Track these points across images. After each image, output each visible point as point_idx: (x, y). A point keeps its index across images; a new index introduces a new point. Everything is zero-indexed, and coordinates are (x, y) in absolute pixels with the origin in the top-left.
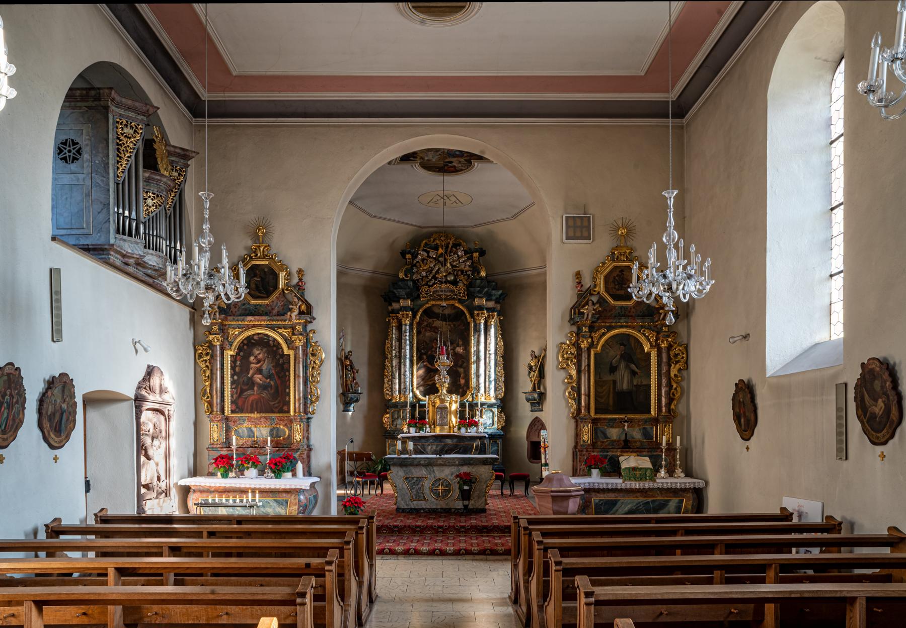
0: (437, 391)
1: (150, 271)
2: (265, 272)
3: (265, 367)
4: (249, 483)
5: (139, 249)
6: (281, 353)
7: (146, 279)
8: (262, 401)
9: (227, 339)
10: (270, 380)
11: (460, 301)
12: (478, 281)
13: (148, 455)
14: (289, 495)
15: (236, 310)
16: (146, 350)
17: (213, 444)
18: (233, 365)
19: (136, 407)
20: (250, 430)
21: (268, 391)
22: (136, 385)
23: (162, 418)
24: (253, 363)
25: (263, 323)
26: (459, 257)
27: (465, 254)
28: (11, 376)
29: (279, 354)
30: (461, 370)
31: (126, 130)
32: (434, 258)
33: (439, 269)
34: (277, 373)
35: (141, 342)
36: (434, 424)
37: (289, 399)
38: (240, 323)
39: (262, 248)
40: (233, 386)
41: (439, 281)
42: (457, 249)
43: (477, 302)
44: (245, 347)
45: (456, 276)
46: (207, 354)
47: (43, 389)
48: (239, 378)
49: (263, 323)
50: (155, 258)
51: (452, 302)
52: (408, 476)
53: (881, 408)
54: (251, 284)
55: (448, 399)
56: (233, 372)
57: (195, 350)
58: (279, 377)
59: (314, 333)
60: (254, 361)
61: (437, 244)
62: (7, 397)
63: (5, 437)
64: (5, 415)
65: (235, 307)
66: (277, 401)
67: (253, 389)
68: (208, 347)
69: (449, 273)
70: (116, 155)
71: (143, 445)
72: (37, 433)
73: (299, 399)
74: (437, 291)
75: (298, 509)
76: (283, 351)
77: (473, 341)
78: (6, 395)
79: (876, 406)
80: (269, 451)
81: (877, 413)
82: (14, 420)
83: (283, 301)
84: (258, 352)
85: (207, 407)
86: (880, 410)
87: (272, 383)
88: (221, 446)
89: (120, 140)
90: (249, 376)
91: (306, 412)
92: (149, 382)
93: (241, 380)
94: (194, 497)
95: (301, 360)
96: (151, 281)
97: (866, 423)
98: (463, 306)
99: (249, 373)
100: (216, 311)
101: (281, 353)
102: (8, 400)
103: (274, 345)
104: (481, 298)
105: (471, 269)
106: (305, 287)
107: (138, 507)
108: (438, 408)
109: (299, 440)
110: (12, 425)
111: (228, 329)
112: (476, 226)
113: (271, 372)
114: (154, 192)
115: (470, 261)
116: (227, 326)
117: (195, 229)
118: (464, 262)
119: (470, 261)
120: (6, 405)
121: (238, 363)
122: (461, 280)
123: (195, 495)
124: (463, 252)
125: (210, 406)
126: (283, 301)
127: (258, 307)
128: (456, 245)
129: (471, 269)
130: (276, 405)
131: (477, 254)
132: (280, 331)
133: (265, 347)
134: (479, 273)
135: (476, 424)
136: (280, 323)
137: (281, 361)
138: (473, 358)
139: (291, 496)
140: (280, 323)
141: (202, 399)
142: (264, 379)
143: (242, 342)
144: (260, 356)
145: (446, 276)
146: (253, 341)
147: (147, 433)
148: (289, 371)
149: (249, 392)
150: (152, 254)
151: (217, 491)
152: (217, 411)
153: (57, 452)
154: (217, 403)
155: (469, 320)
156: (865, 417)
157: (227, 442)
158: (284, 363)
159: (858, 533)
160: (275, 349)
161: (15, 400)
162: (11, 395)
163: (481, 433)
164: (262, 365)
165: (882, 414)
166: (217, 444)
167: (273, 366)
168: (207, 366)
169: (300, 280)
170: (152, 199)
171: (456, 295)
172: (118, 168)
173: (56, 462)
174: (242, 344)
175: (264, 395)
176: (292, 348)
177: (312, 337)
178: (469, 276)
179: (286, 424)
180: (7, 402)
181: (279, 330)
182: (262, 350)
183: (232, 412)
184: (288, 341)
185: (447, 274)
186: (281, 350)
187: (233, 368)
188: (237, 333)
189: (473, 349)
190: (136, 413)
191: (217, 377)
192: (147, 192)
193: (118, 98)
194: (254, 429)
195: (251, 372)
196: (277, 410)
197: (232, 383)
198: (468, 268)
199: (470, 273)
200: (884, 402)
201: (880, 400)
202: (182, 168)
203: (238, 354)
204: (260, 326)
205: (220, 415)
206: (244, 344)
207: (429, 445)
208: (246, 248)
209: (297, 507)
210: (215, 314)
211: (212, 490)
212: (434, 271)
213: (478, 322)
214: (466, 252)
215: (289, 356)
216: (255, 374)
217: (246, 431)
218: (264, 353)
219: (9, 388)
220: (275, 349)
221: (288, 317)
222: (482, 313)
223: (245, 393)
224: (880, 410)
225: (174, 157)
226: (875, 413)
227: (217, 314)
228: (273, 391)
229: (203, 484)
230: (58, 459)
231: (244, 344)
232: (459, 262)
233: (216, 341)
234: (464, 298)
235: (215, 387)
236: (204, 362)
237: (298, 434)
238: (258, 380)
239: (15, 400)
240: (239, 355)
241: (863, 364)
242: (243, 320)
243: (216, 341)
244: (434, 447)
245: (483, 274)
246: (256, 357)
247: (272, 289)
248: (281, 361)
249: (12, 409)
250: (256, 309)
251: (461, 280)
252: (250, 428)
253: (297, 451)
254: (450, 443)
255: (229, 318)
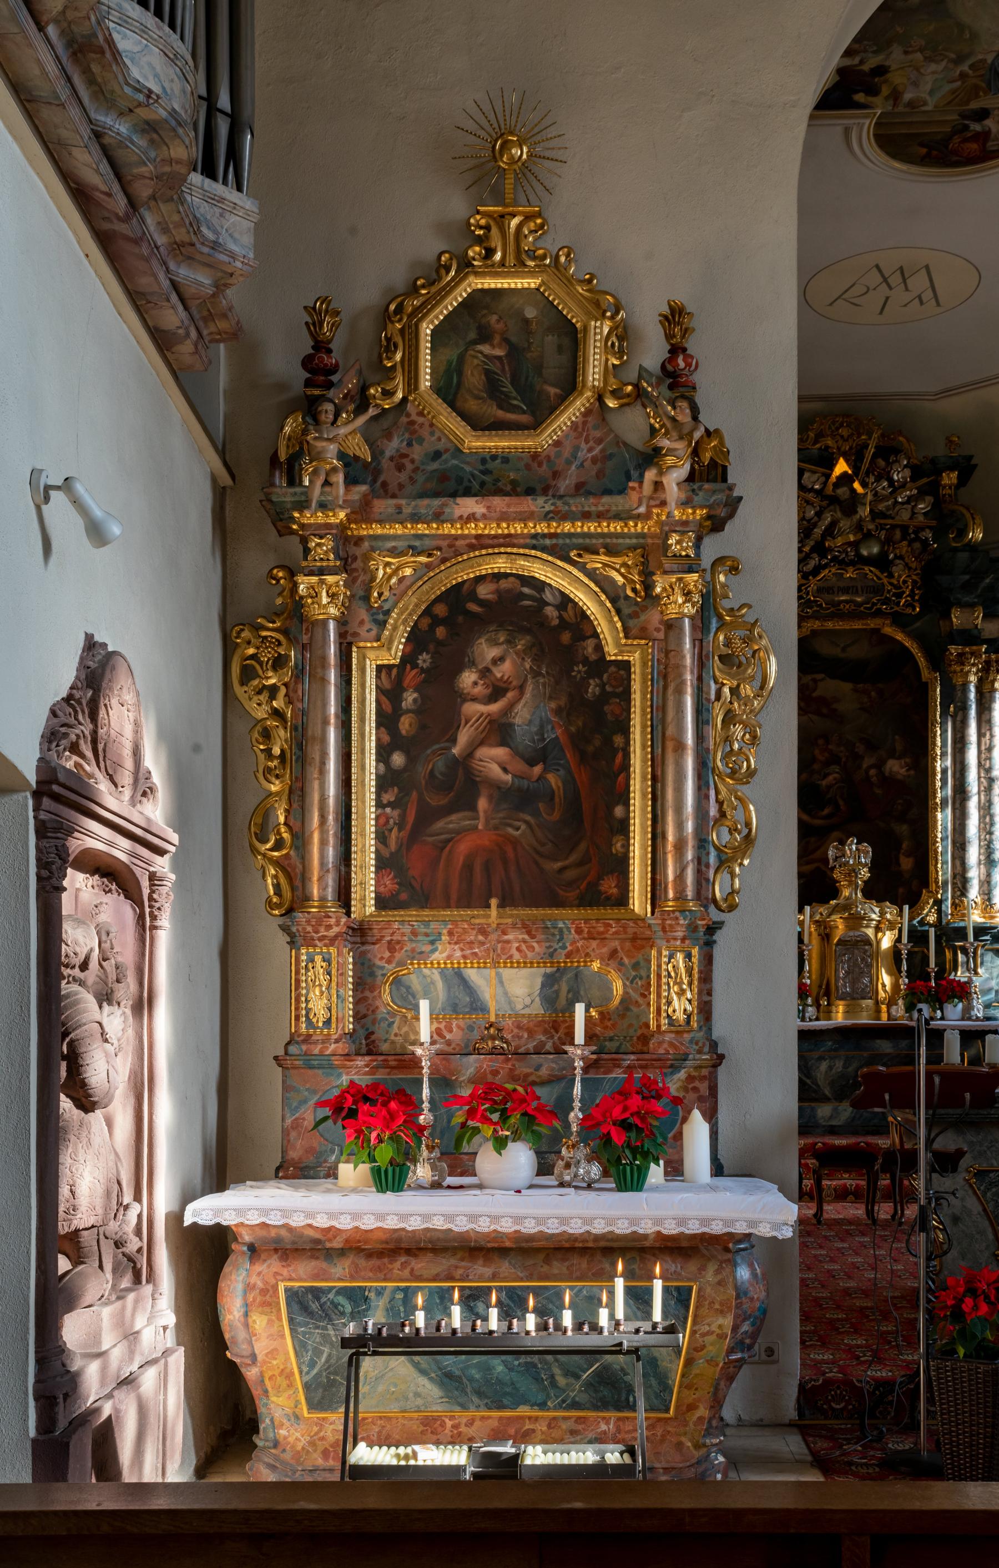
0: (835, 893)
1: (122, 128)
2: (527, 322)
3: (522, 715)
4: (423, 1209)
6: (593, 657)
8: (511, 854)
9: (366, 598)
10: (545, 770)
11: (899, 620)
12: (963, 556)
13: (83, 1084)
14: (692, 1266)
15: (403, 477)
16: (96, 533)
17: (307, 1039)
18: (387, 707)
19: (42, 831)
20: (457, 979)
21: (536, 814)
22: (38, 721)
23: (128, 911)
24: (474, 699)
25: (518, 528)
26: (896, 488)
27: (914, 478)
29: (585, 661)
30: (903, 829)
32: (816, 491)
33: (834, 524)
34: (578, 740)
35: (79, 488)
36: (828, 994)
37: (627, 846)
38: (421, 528)
39: (515, 222)
40: (388, 797)
41: (835, 559)
42: (889, 464)
43: (957, 618)
44: (441, 632)
45: (888, 542)
46: (278, 663)
48: (411, 760)
49: (518, 528)
50: (155, 58)
51: (872, 624)
52: (984, 1167)
54: (468, 371)
55: (874, 916)
56: (386, 738)
57: (229, 648)
58: (583, 757)
59: (734, 570)
60: (479, 690)
61: (827, 447)
65: (400, 468)
66: (573, 858)
67: (473, 808)
68: (284, 631)
69: (868, 536)
71: (65, 1034)
73: (680, 847)
74: (829, 590)
75: (735, 1328)
76: (599, 648)
77: (942, 738)
80: (579, 1064)
83: (599, 441)
84: (493, 652)
85: (277, 887)
87: (553, 780)
88: (342, 1048)
90: (455, 751)
91: (704, 896)
92: (94, 717)
93: (422, 771)
94: (254, 1279)
95: (688, 677)
98: (909, 635)
99: (454, 741)
100: (334, 470)
101: (593, 657)
103: (564, 625)
104: (972, 606)
105: (934, 523)
106: (697, 378)
107: (40, 1361)
108: (840, 942)
109: (680, 1016)
111: (367, 558)
112: (947, 393)
113: (549, 736)
115: (929, 499)
116: (366, 544)
118: (908, 502)
119: (929, 499)
121: (409, 698)
122: (901, 557)
123: (259, 1267)
124: (907, 472)
125: (290, 878)
126: (599, 441)
127: (491, 465)
128: (888, 452)
129: (934, 523)
130: (571, 874)
131: (954, 475)
132: (596, 562)
133: (528, 631)
134: (962, 532)
135: (963, 992)
136: (591, 527)
137: (593, 689)
138: (943, 791)
139: (703, 1268)
140: (591, 527)
141: (254, 851)
142: (520, 766)
143: (427, 612)
144: (505, 670)
145: (856, 545)
146: (473, 607)
147: (76, 972)
148: (624, 729)
149: (455, 821)
151: (359, 1250)
152: (323, 899)
154: (322, 863)
155: (926, 674)
157: (362, 1033)
158: (604, 697)
160: (566, 637)
163: (978, 1019)
164: (511, 706)
166: (326, 1040)
167: (558, 712)
168: (277, 713)
169: (676, 350)
171: (886, 601)
174: (426, 622)
175: (519, 831)
176: (643, 633)
177: (723, 586)
178: (925, 543)
179: (613, 954)
181: (587, 558)
182: (508, 642)
183: (382, 903)
184: (622, 603)
185: (859, 536)
186: (590, 643)
187: (386, 720)
188: (408, 572)
189: (942, 763)
190: (41, 864)
191: (324, 755)
194: (472, 974)
195: (464, 737)
196: (572, 895)
197: (383, 784)
198: (921, 518)
199: (929, 534)
203: (408, 659)
204: (508, 540)
205: (337, 923)
206: (437, 621)
207: (821, 1058)
208: (442, 228)
209: (727, 1322)
210: (327, 483)
211: (337, 1244)
212: (818, 531)
213: (959, 681)
214: (917, 472)
215: (626, 665)
216: (482, 743)
217: (440, 985)
218: (522, 655)
220: (566, 637)
221: (647, 488)
222: (972, 654)
223: (440, 824)
227: (339, 478)
228: (556, 816)
229: (297, 1221)
231: (437, 621)
232: (896, 502)
233: (325, 600)
234: (909, 611)
235: (316, 797)
236: (264, 697)
237: (681, 993)
238: (495, 771)
240: (414, 666)
242: (439, 517)
243: (325, 600)
244: (839, 1065)
245: (976, 535)
246: (485, 673)
247: (553, 391)
248: (593, 689)
250: (486, 472)
251: (901, 557)
252: (459, 975)
253: (675, 1069)
254: (889, 1050)
255: (383, 506)
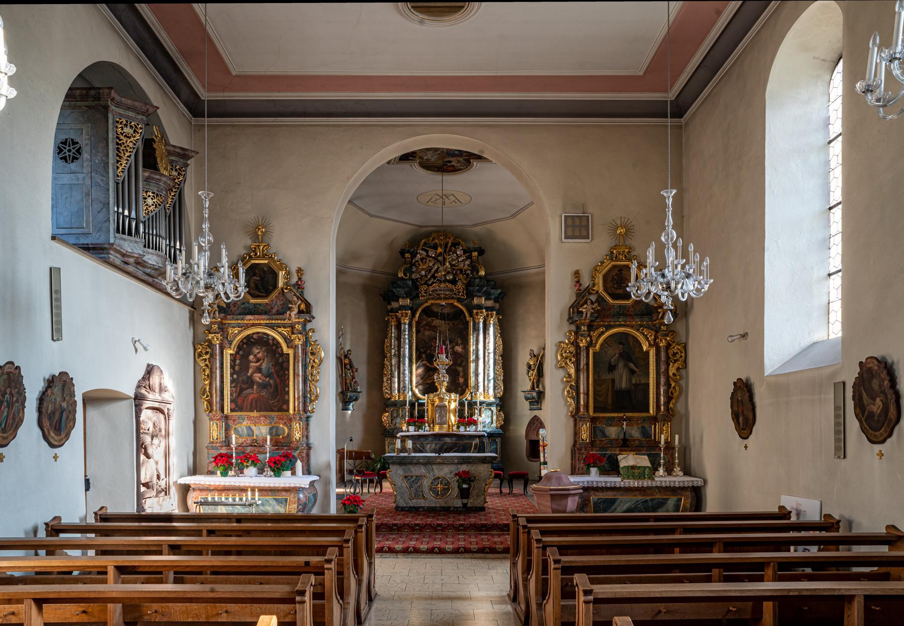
0: (436, 390)
1: (149, 270)
2: (264, 271)
3: (264, 366)
4: (248, 481)
5: (138, 248)
6: (281, 352)
7: (146, 278)
8: (262, 400)
9: (227, 338)
10: (270, 379)
11: (459, 300)
12: (477, 281)
13: (148, 454)
14: (289, 494)
15: (236, 309)
16: (145, 349)
17: (212, 443)
18: (233, 364)
19: (136, 406)
20: (249, 428)
21: (267, 389)
22: (135, 384)
23: (162, 416)
24: (253, 362)
25: (262, 322)
26: (458, 257)
27: (464, 254)
28: (11, 375)
29: (279, 353)
30: (460, 369)
31: (125, 130)
32: (433, 257)
33: (438, 268)
34: (277, 372)
35: (141, 341)
36: (433, 422)
37: (289, 397)
38: (240, 322)
39: (261, 248)
40: (233, 385)
41: (438, 280)
42: (456, 249)
43: (476, 301)
44: (245, 346)
45: (455, 275)
46: (207, 353)
47: (43, 388)
48: (238, 376)
49: (262, 322)
50: (155, 258)
51: (451, 301)
52: (407, 475)
53: (879, 406)
54: (251, 283)
55: (447, 398)
56: (232, 371)
57: (195, 349)
58: (278, 376)
59: (313, 331)
60: (254, 360)
61: (436, 243)
62: (7, 396)
63: (5, 435)
64: (5, 414)
65: (235, 306)
66: (276, 400)
67: (253, 388)
68: (208, 345)
69: (449, 273)
70: (115, 155)
71: (143, 444)
72: (37, 431)
73: (299, 398)
74: (436, 290)
75: (298, 507)
76: (282, 350)
77: (472, 340)
78: (6, 394)
79: (874, 405)
80: (268, 449)
81: (875, 411)
82: (14, 418)
83: (282, 300)
84: (257, 351)
85: (207, 406)
86: (878, 409)
87: (271, 381)
88: (220, 445)
89: (120, 140)
90: (249, 374)
91: (305, 411)
92: (149, 380)
93: (241, 379)
94: (194, 496)
95: (300, 359)
96: (150, 280)
97: (864, 422)
98: (462, 305)
99: (248, 372)
100: (216, 310)
101: (281, 352)
102: (8, 399)
103: (273, 344)
104: (480, 297)
105: (470, 268)
106: (305, 286)
107: (137, 505)
108: (437, 406)
109: (298, 438)
110: (12, 424)
111: (227, 328)
112: (475, 225)
113: (270, 371)
114: (154, 191)
115: (469, 260)
116: (227, 325)
117: (195, 228)
118: (463, 261)
119: (469, 260)
120: (6, 404)
121: (238, 362)
122: (460, 279)
123: (194, 493)
124: (462, 252)
125: (210, 404)
126: (282, 300)
127: (257, 306)
128: (455, 245)
129: (470, 268)
130: (276, 404)
131: (476, 253)
132: (280, 330)
133: (265, 346)
134: (478, 272)
135: (475, 423)
136: (279, 322)
137: (281, 360)
138: (472, 357)
139: (291, 494)
140: (279, 322)
141: (201, 398)
142: (263, 378)
143: (242, 341)
144: (260, 355)
145: (445, 275)
146: (252, 340)
147: (147, 431)
148: (288, 370)
149: (249, 391)
150: (152, 254)
151: (217, 490)
152: (216, 410)
153: (56, 450)
154: (216, 402)
155: (468, 319)
156: (863, 416)
157: (227, 441)
158: (283, 362)
159: (856, 531)
160: (274, 347)
161: (15, 399)
162: (11, 394)
163: (480, 431)
164: (261, 364)
165: (880, 413)
166: (217, 443)
167: (272, 365)
168: (206, 365)
169: (300, 279)
170: (152, 199)
171: (455, 294)
172: (118, 168)
173: (56, 461)
174: (241, 343)
175: (264, 394)
176: (292, 347)
177: (311, 336)
178: (468, 275)
179: (285, 423)
180: (7, 401)
181: (279, 329)
182: (261, 349)
183: (232, 410)
184: (287, 340)
185: (446, 273)
186: (280, 349)
187: (232, 367)
188: (237, 332)
189: (472, 348)
190: (136, 412)
191: (216, 376)
192: (146, 192)
193: (117, 98)
194: (253, 427)
195: (250, 371)
196: (276, 409)
197: (232, 382)
198: (467, 267)
199: (469, 272)
200: (882, 401)
201: (878, 399)
202: (182, 168)
203: (237, 353)
204: (260, 325)
205: (219, 414)
206: (244, 343)
207: (428, 444)
208: (246, 247)
209: (296, 506)
210: (214, 313)
211: (212, 488)
212: (433, 271)
213: (477, 321)
214: (465, 252)
215: (288, 354)
216: (255, 373)
217: (245, 430)
218: (264, 352)
219: (9, 386)
220: (274, 347)
221: (288, 316)
222: (481, 312)
223: (245, 392)
224: (878, 409)
225: (173, 156)
226: (873, 412)
227: (217, 313)
228: (272, 390)
229: (202, 483)
230: (58, 457)
231: (244, 343)
232: (458, 261)
233: (215, 340)
234: (463, 297)
235: (214, 386)
236: (203, 361)
237: (298, 433)
238: (258, 379)
239: (15, 399)
240: (239, 354)
241: (861, 363)
242: (242, 319)
243: (215, 340)
244: (433, 446)
245: (482, 273)
246: (255, 356)
247: (271, 288)
248: (281, 360)
249: (12, 408)
250: (255, 308)
251: (460, 279)
252: (250, 427)
253: (296, 450)
254: (449, 441)
255: (229, 317)
